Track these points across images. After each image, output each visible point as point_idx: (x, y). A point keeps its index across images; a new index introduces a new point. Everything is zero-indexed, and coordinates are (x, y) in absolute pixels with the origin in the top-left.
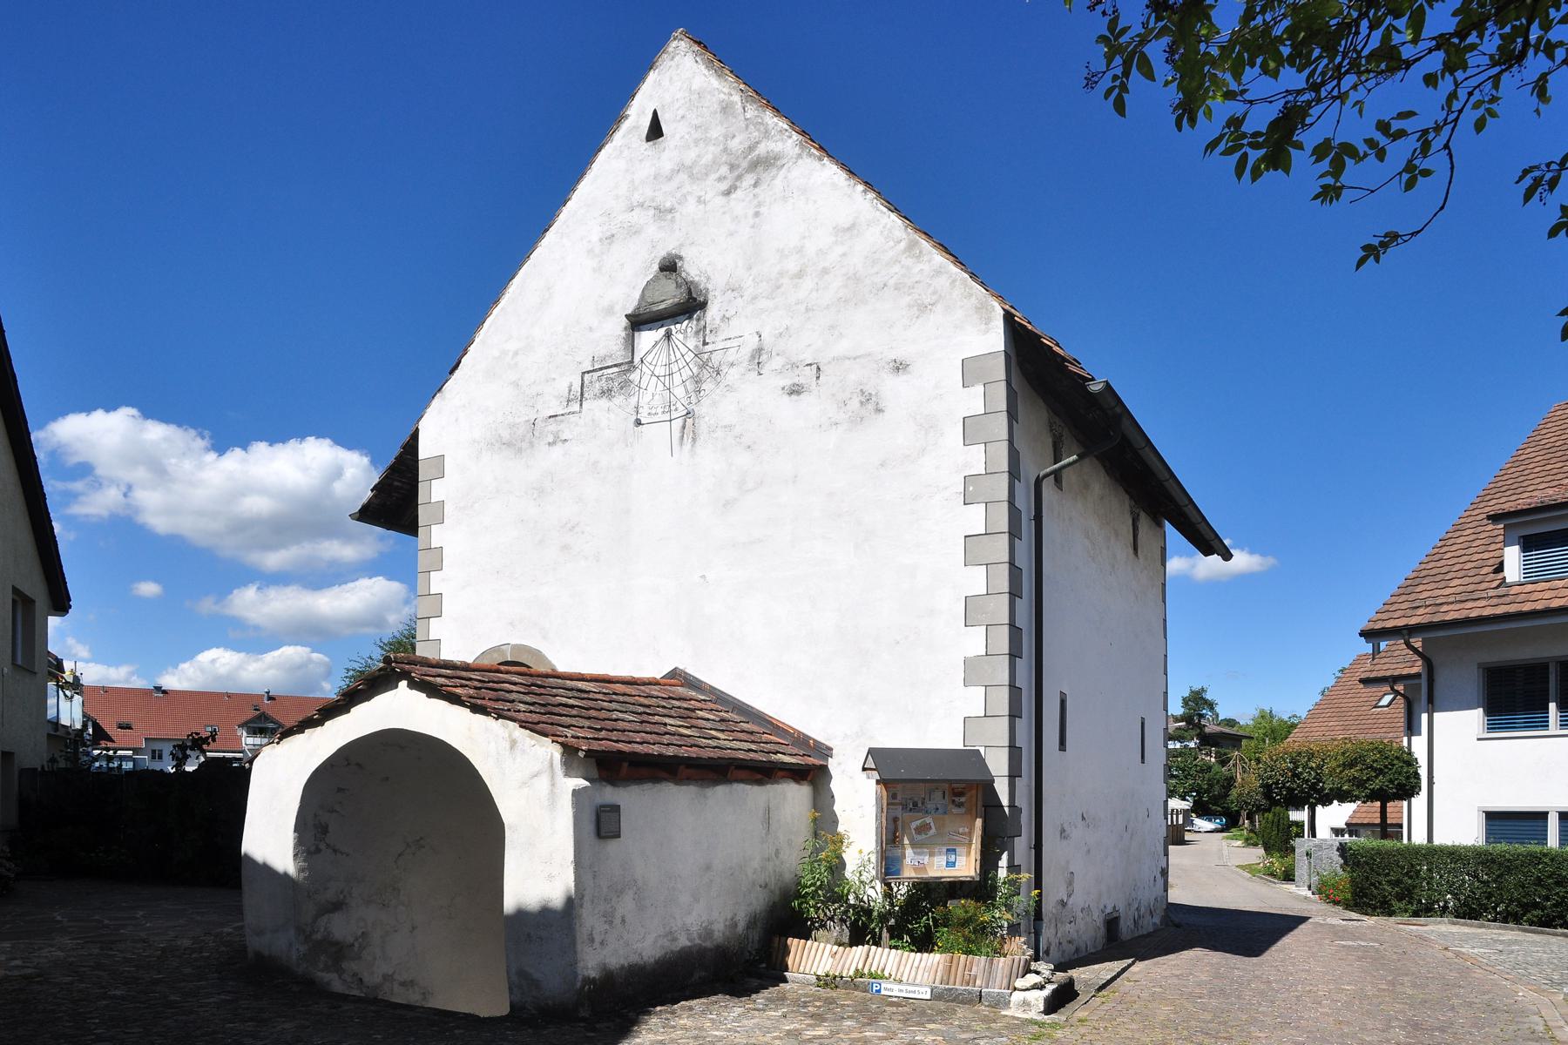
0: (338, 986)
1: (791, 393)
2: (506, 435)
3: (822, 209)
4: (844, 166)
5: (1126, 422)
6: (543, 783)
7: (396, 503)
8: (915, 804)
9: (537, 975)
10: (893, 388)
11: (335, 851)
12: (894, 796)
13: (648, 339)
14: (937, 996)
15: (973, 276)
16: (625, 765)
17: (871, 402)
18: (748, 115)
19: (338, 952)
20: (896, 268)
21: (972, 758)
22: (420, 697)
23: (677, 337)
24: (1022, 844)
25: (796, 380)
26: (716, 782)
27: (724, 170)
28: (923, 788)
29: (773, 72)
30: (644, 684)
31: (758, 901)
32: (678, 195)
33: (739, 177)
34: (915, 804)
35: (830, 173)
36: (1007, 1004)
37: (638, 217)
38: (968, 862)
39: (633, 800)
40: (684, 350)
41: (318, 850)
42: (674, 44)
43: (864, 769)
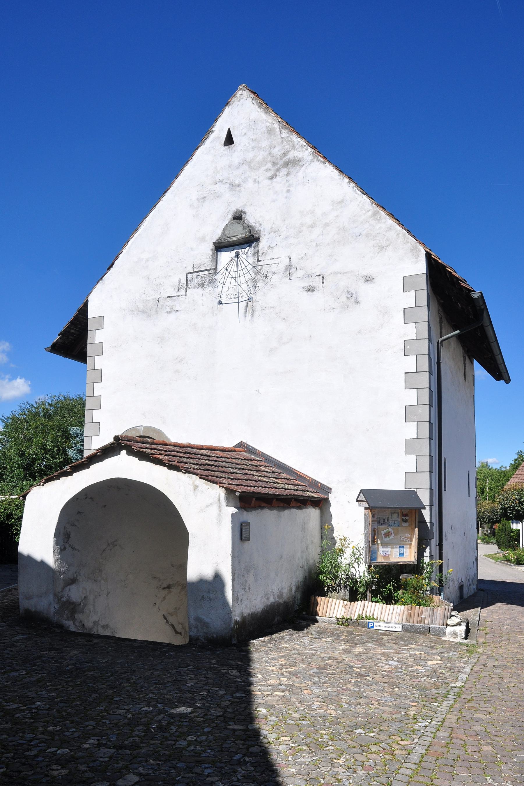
0: (72, 628)
1: (308, 290)
2: (141, 306)
3: (324, 188)
4: (337, 168)
5: (485, 314)
6: (214, 509)
7: (74, 342)
8: (384, 521)
9: (207, 620)
10: (365, 291)
11: (104, 550)
12: (373, 516)
13: (225, 256)
14: (405, 629)
15: (409, 232)
16: (254, 499)
17: (352, 297)
18: (283, 136)
19: (72, 608)
20: (367, 225)
21: (412, 495)
22: (135, 460)
23: (242, 256)
24: (434, 542)
25: (311, 284)
26: (284, 508)
27: (269, 165)
28: (388, 511)
29: (300, 112)
30: (229, 451)
31: (299, 576)
32: (243, 177)
33: (278, 170)
34: (384, 521)
35: (329, 171)
36: (444, 634)
37: (219, 188)
38: (410, 553)
39: (263, 519)
40: (247, 264)
41: (65, 548)
42: (240, 92)
43: (357, 501)
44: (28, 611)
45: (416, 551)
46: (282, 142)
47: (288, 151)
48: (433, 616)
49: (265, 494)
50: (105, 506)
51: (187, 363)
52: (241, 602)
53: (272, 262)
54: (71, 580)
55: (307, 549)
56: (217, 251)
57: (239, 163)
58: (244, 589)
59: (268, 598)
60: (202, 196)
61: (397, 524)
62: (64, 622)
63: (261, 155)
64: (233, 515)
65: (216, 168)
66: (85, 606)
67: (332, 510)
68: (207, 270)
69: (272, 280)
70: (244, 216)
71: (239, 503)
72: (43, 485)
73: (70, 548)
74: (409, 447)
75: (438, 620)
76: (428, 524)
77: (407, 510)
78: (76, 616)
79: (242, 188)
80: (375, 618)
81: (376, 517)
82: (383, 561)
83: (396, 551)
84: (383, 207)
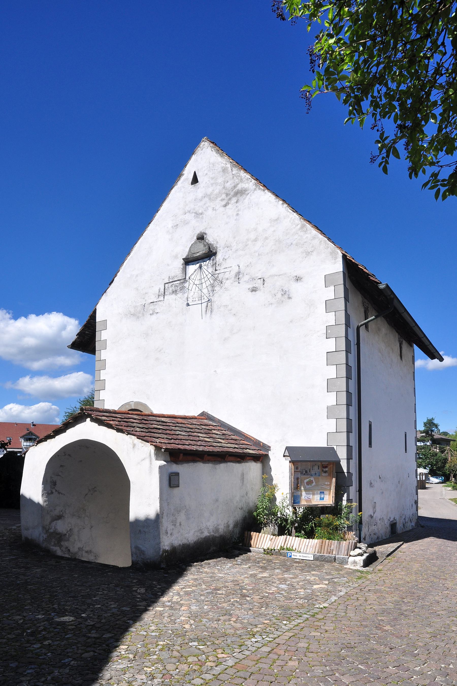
2: (132, 311)
3: (265, 209)
6: (147, 461)
8: (306, 472)
9: (143, 549)
10: (295, 288)
11: (86, 495)
13: (192, 268)
14: (316, 559)
15: (329, 239)
16: (182, 455)
17: (286, 294)
18: (234, 173)
19: (60, 538)
21: (331, 451)
22: (95, 425)
23: (204, 267)
24: (353, 490)
26: (221, 462)
28: (309, 464)
30: (190, 419)
31: (238, 515)
32: (205, 207)
33: (230, 199)
34: (306, 472)
35: (267, 197)
37: (189, 217)
38: (329, 498)
39: (185, 470)
40: (207, 273)
41: (52, 493)
42: (203, 143)
43: (284, 456)
44: (27, 539)
45: (334, 496)
46: (233, 177)
47: (238, 184)
48: (339, 548)
49: (191, 450)
50: (81, 461)
51: (164, 352)
52: (175, 536)
53: (226, 270)
54: (58, 516)
55: (246, 495)
56: (186, 265)
57: (202, 197)
58: (175, 525)
59: (202, 533)
60: (176, 224)
61: (317, 474)
62: (52, 547)
63: (218, 189)
64: (160, 467)
65: (186, 202)
66: (70, 536)
67: (271, 463)
68: (178, 280)
69: (226, 284)
70: (205, 237)
71: (169, 458)
72: (36, 446)
73: (57, 493)
74: (331, 412)
75: (343, 551)
76: (346, 474)
77: (327, 463)
78: (62, 543)
79: (204, 216)
80: (294, 549)
81: (299, 469)
82: (306, 504)
83: (317, 497)
84: (308, 221)
